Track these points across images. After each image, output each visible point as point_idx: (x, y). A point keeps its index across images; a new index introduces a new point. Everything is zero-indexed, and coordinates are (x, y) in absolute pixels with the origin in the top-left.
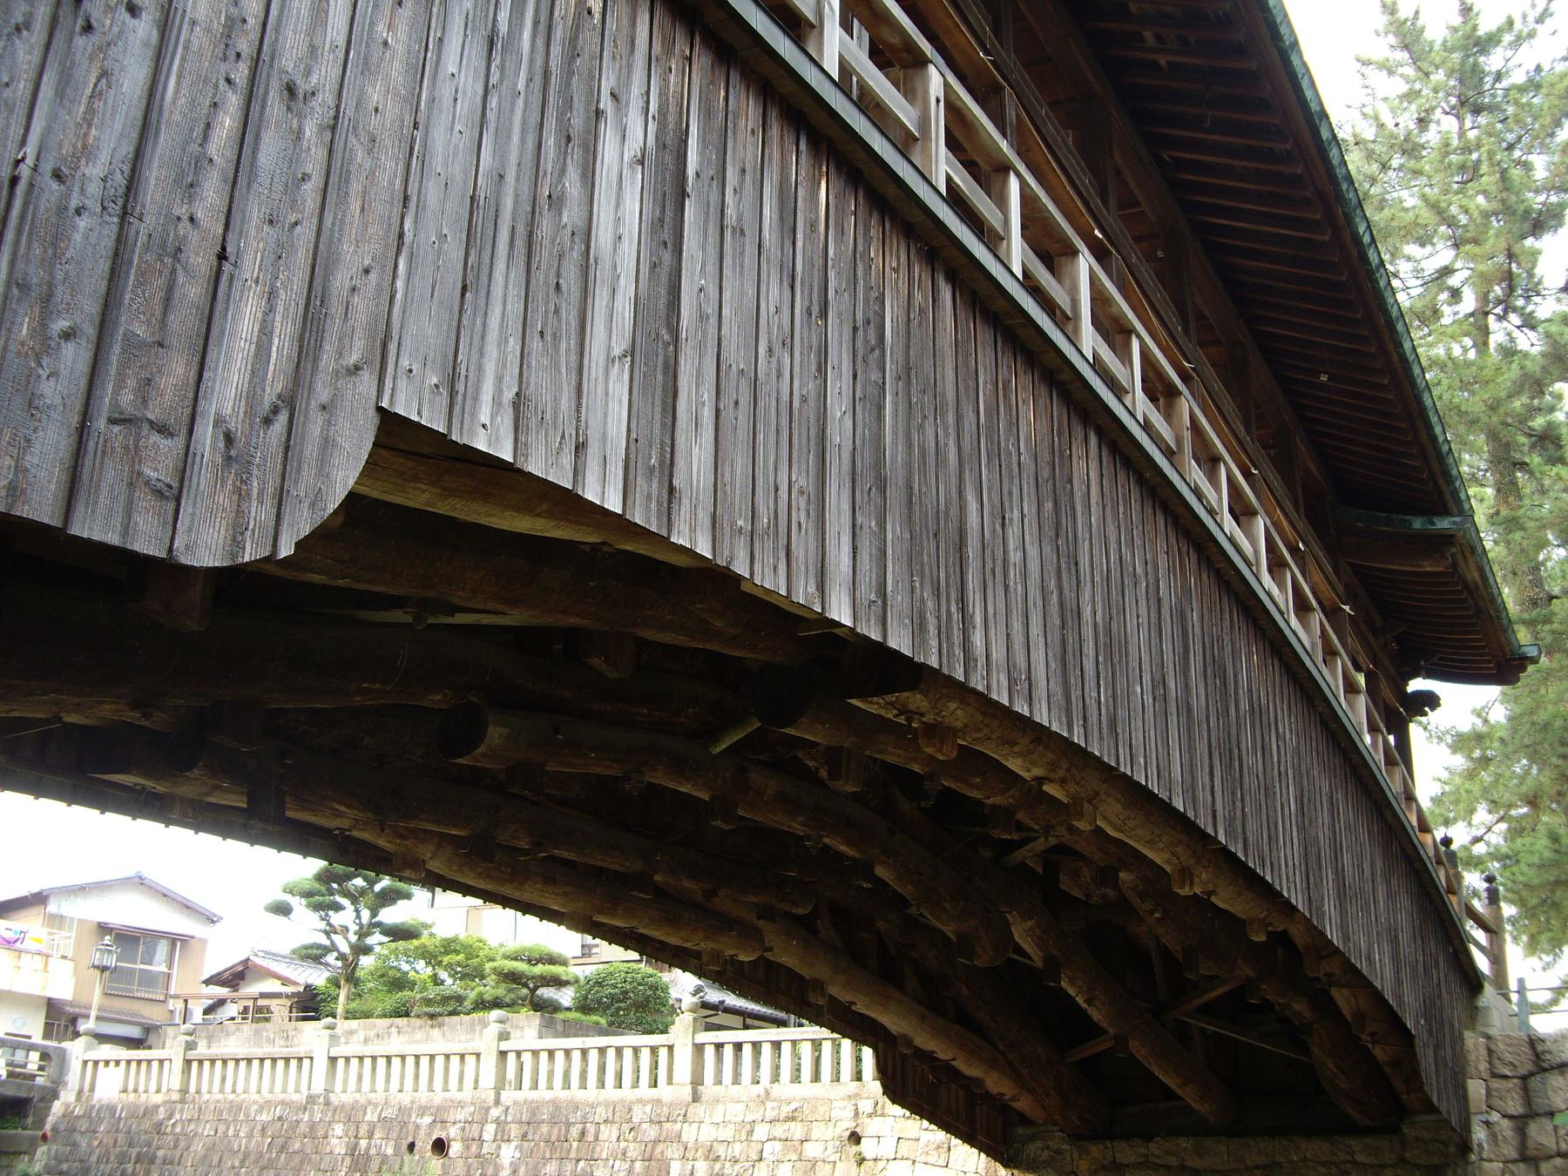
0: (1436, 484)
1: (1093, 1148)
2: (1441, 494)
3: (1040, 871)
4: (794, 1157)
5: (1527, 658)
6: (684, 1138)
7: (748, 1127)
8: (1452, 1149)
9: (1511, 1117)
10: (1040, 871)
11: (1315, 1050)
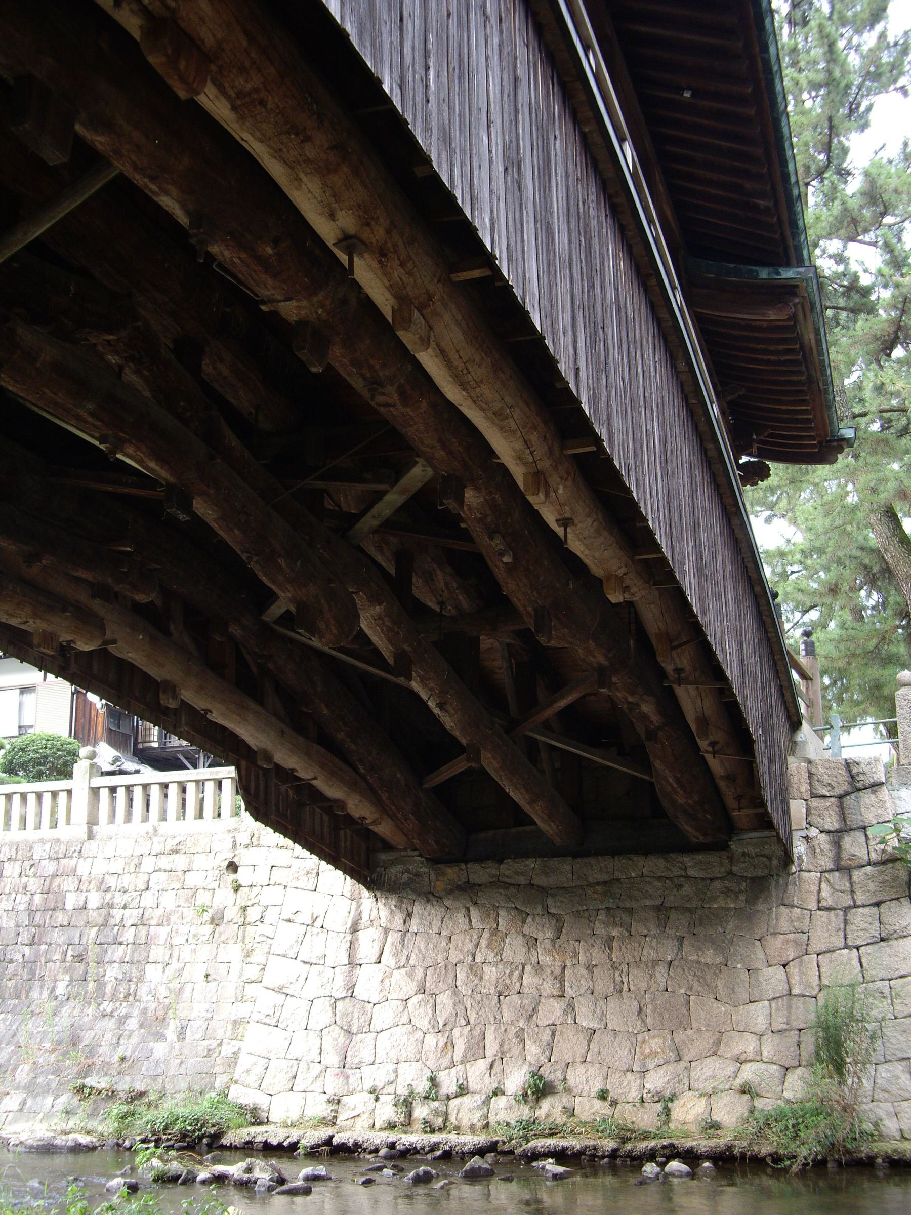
0: (783, 236)
1: (449, 871)
2: (786, 248)
3: (393, 572)
4: (177, 885)
5: (844, 440)
6: (79, 872)
7: (136, 861)
8: (775, 862)
9: (829, 832)
10: (393, 572)
11: (657, 764)
